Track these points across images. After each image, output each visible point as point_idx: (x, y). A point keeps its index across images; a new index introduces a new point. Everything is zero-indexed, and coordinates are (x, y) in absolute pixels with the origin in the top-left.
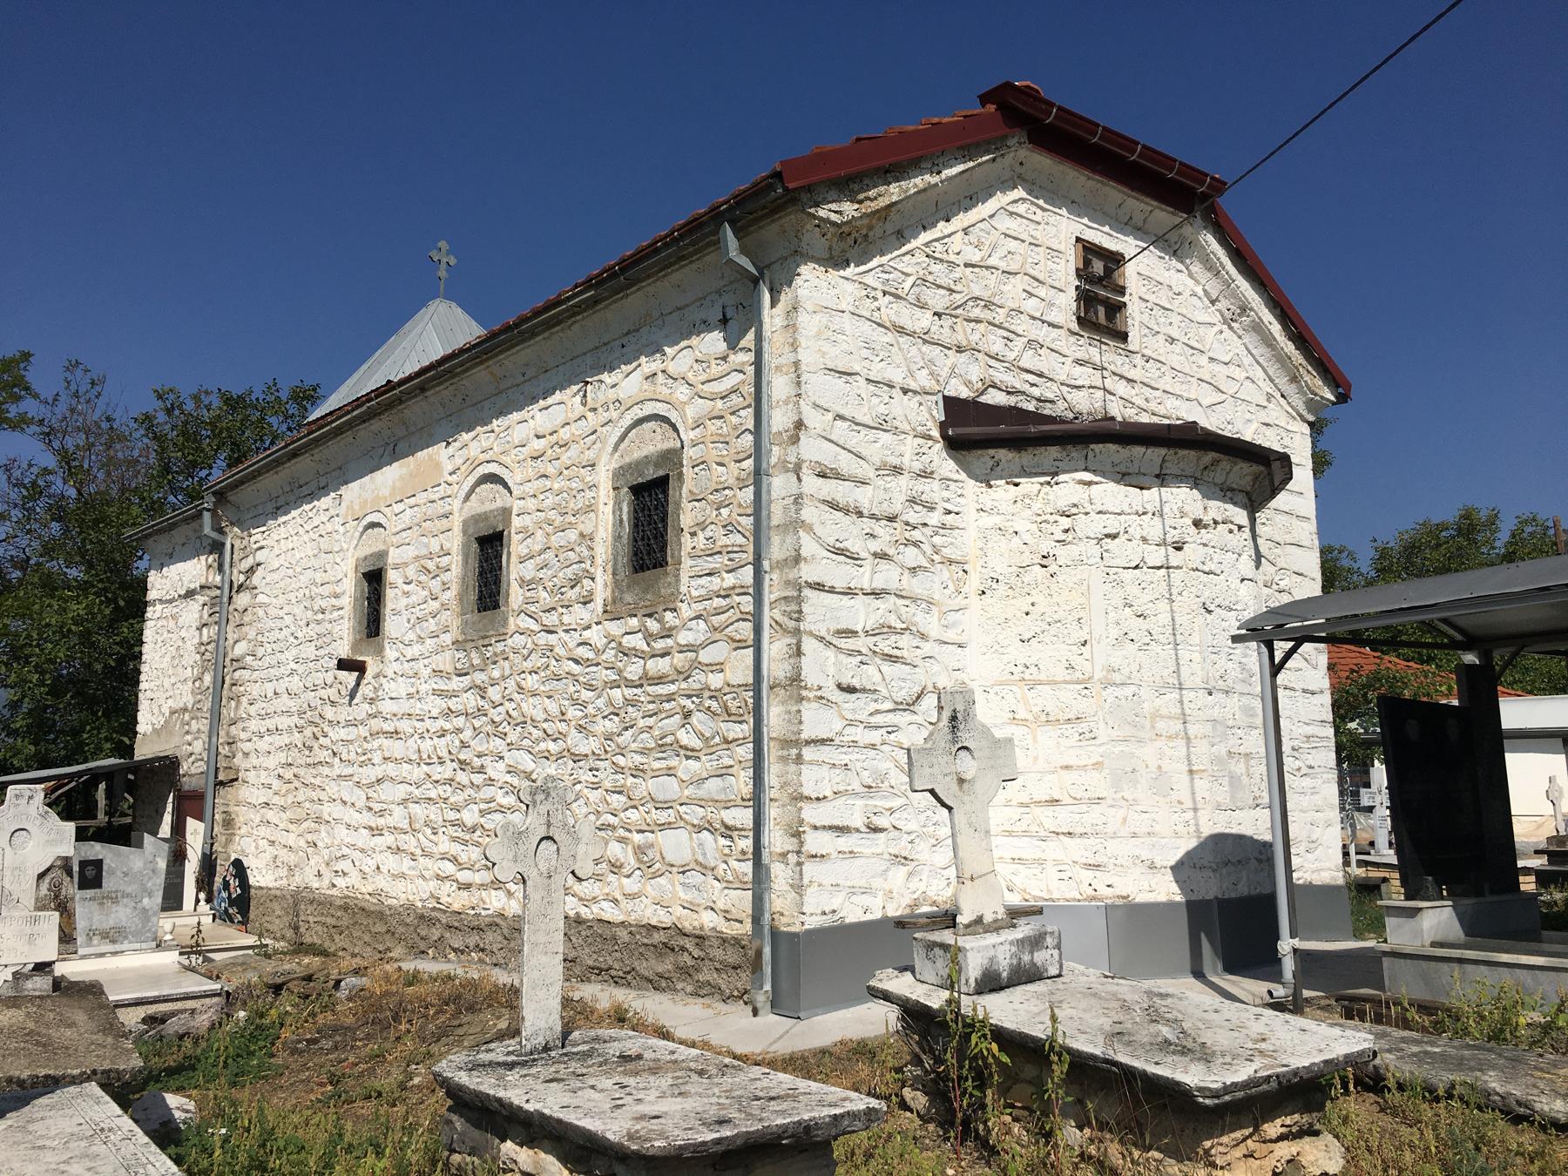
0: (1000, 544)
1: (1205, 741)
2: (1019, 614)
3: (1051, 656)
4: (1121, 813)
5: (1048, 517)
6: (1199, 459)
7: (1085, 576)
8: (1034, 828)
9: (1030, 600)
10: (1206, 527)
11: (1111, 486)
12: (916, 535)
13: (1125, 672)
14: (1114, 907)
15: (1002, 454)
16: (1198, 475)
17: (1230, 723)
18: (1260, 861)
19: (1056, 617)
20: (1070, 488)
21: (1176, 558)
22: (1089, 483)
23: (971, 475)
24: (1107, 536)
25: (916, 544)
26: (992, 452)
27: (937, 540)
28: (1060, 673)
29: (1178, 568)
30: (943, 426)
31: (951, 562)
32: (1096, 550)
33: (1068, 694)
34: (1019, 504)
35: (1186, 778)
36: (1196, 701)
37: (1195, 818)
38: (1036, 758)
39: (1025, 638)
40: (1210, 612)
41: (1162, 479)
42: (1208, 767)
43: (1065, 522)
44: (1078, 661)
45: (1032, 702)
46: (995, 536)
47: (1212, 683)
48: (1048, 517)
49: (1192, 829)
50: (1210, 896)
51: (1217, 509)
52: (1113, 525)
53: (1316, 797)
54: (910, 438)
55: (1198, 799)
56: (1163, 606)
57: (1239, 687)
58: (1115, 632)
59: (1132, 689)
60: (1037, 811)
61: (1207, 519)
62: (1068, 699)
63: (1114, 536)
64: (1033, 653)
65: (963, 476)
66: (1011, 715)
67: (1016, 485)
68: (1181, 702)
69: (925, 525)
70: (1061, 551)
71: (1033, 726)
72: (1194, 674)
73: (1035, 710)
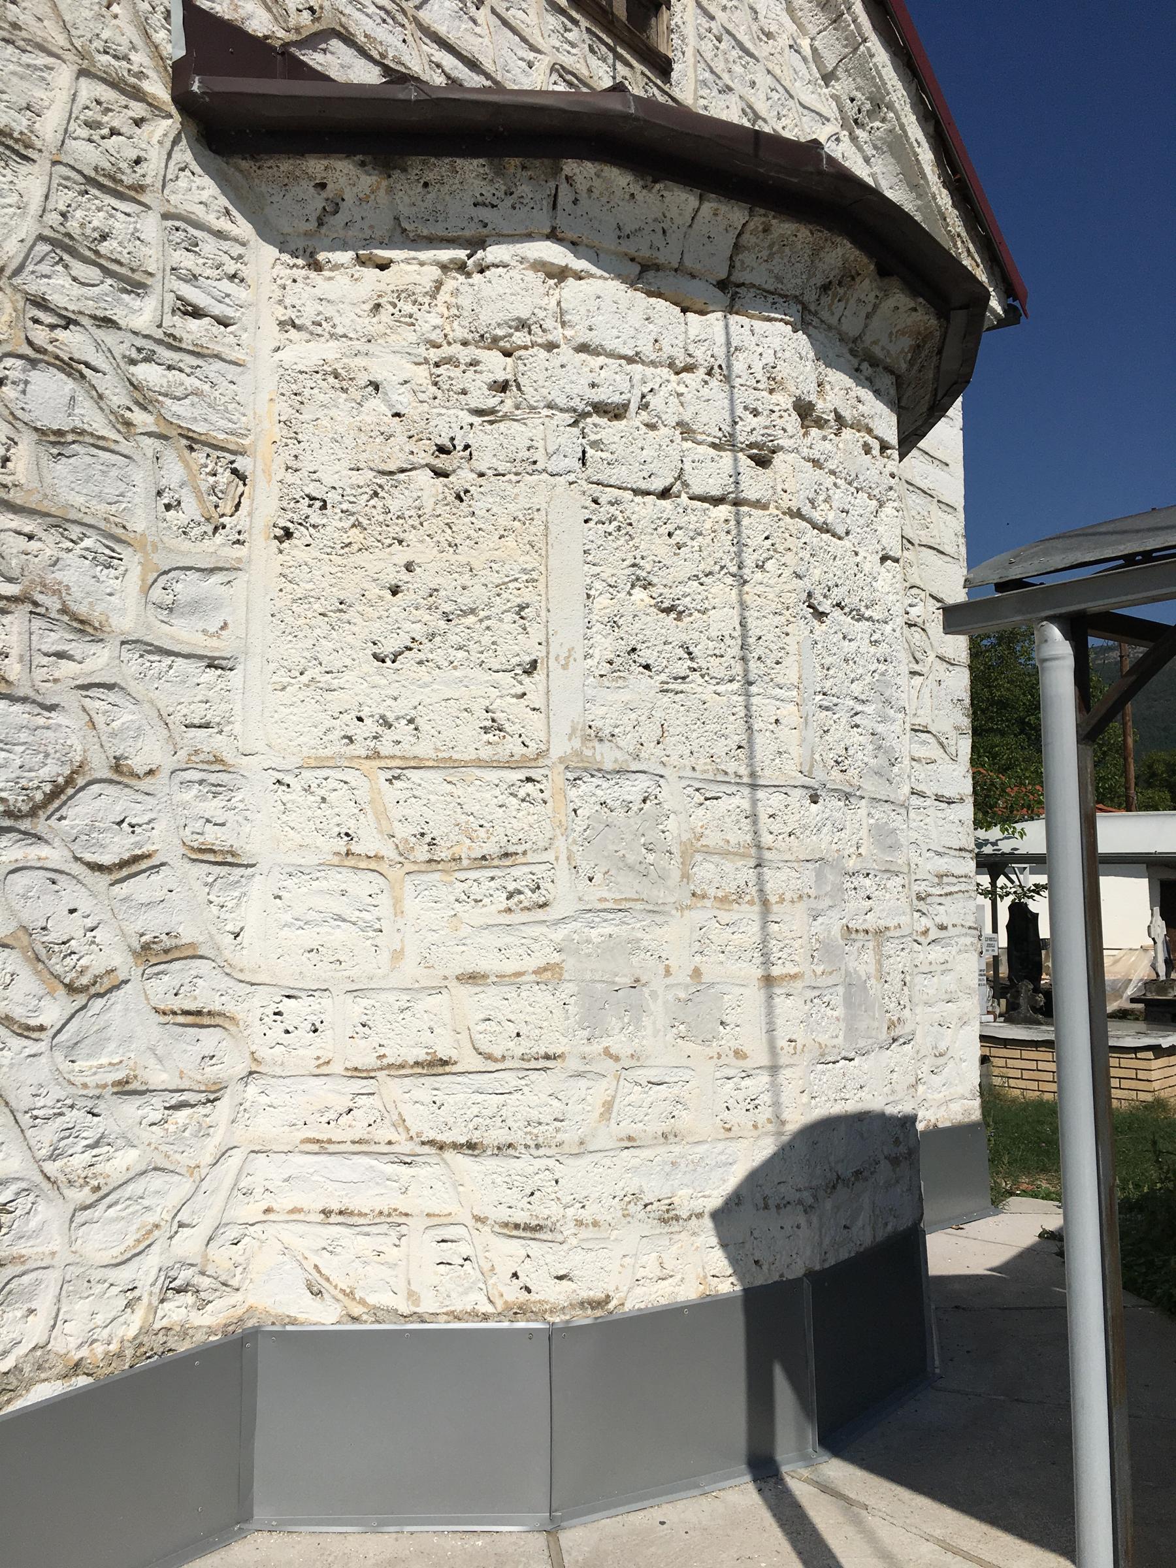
0: (338, 415)
1: (801, 906)
2: (374, 591)
3: (445, 699)
4: (600, 1091)
5: (455, 349)
6: (816, 252)
7: (539, 501)
8: (384, 1133)
9: (401, 555)
10: (820, 423)
11: (613, 289)
12: (74, 342)
13: (627, 742)
14: (568, 1331)
15: (345, 175)
16: (810, 296)
17: (851, 864)
18: (895, 1161)
19: (465, 601)
20: (514, 279)
21: (755, 483)
22: (560, 274)
23: (267, 232)
24: (600, 409)
25: (70, 367)
26: (315, 166)
27: (148, 374)
28: (469, 741)
29: (759, 505)
30: (179, 73)
31: (193, 442)
32: (570, 440)
33: (484, 795)
34: (385, 315)
35: (755, 995)
36: (785, 811)
37: (775, 1088)
38: (397, 955)
39: (389, 646)
40: (820, 615)
41: (732, 294)
42: (804, 967)
43: (496, 365)
44: (509, 710)
45: (396, 812)
46: (321, 392)
47: (820, 775)
48: (455, 349)
49: (765, 1113)
50: (797, 1271)
51: (842, 392)
52: (614, 384)
53: (948, 978)
54: (64, 75)
55: (782, 1043)
56: (721, 591)
57: (871, 786)
58: (605, 645)
59: (643, 784)
60: (393, 1088)
61: (823, 407)
62: (488, 806)
63: (616, 412)
64: (409, 688)
65: (243, 228)
66: (341, 845)
67: (383, 267)
68: (753, 817)
69: (107, 322)
70: (483, 437)
71: (396, 873)
72: (785, 749)
73: (403, 832)
